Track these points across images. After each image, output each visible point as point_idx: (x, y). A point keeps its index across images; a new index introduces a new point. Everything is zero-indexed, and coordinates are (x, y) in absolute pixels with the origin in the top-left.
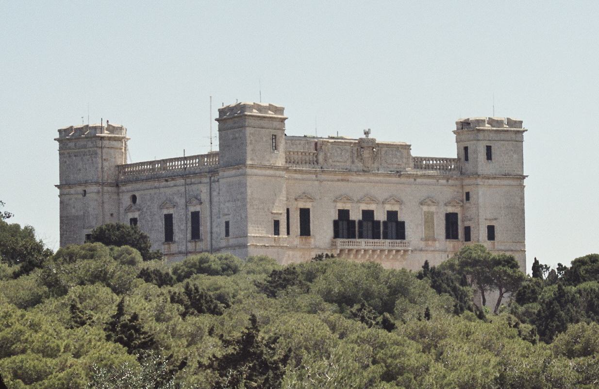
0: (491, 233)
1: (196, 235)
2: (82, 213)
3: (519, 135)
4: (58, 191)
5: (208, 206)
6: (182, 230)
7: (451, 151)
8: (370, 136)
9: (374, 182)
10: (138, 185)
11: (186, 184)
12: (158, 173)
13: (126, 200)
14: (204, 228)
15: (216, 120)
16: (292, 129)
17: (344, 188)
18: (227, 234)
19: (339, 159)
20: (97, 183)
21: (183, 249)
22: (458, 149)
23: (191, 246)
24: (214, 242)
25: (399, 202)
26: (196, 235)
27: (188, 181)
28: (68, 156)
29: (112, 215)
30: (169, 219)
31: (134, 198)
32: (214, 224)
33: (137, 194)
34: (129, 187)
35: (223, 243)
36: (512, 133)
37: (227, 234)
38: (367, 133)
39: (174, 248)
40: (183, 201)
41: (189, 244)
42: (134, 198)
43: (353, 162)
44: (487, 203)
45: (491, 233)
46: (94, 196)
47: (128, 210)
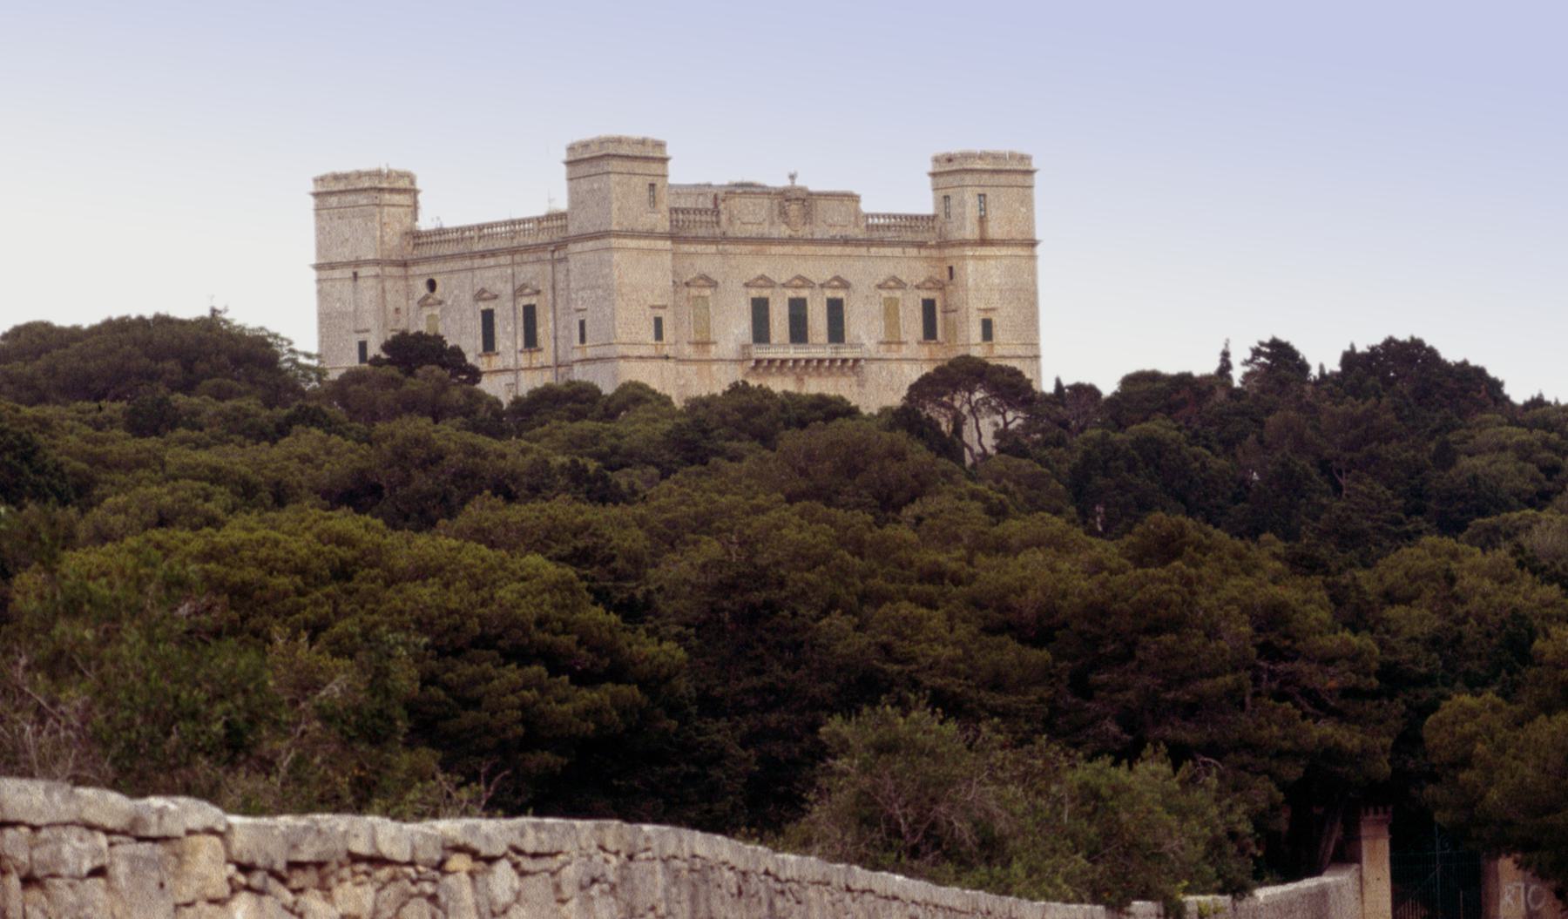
0: (987, 327)
1: (531, 341)
2: (351, 309)
3: (1027, 178)
4: (313, 274)
5: (550, 297)
6: (508, 335)
7: (922, 202)
8: (798, 183)
9: (1491, 450)
10: (439, 267)
11: (513, 264)
12: (473, 246)
13: (421, 289)
14: (544, 330)
15: (1352, 347)
16: (680, 173)
17: (761, 267)
18: (583, 339)
19: (750, 218)
20: (376, 262)
21: (511, 363)
22: (936, 199)
23: (523, 361)
24: (560, 352)
25: (845, 285)
26: (531, 341)
27: (517, 258)
28: (754, 883)
29: (397, 310)
30: (488, 317)
31: (432, 285)
32: (561, 325)
33: (438, 279)
34: (425, 269)
35: (577, 355)
36: (1015, 173)
37: (583, 339)
38: (792, 177)
39: (497, 363)
40: (509, 289)
41: (520, 356)
42: (432, 285)
43: (772, 223)
44: (981, 278)
45: (987, 327)
46: (371, 282)
47: (423, 303)
